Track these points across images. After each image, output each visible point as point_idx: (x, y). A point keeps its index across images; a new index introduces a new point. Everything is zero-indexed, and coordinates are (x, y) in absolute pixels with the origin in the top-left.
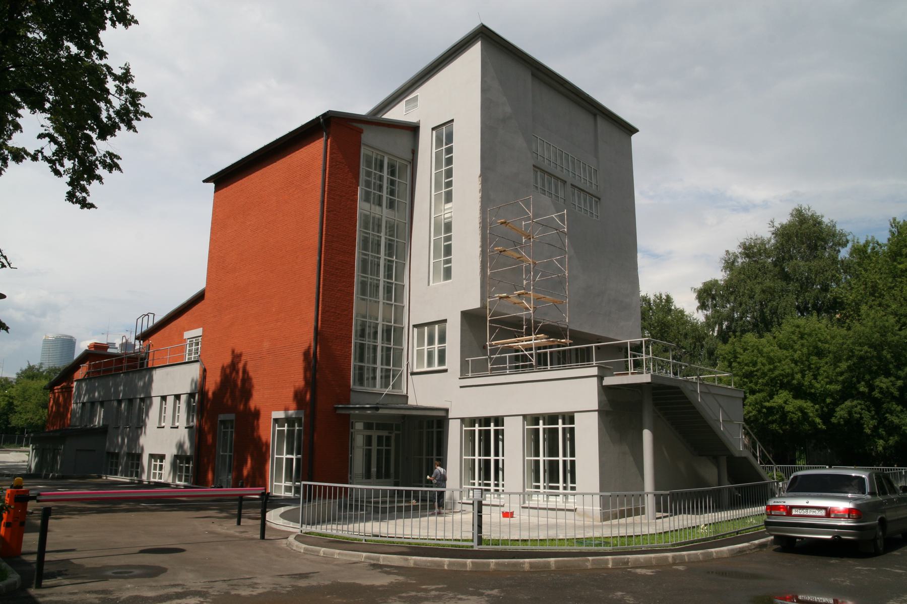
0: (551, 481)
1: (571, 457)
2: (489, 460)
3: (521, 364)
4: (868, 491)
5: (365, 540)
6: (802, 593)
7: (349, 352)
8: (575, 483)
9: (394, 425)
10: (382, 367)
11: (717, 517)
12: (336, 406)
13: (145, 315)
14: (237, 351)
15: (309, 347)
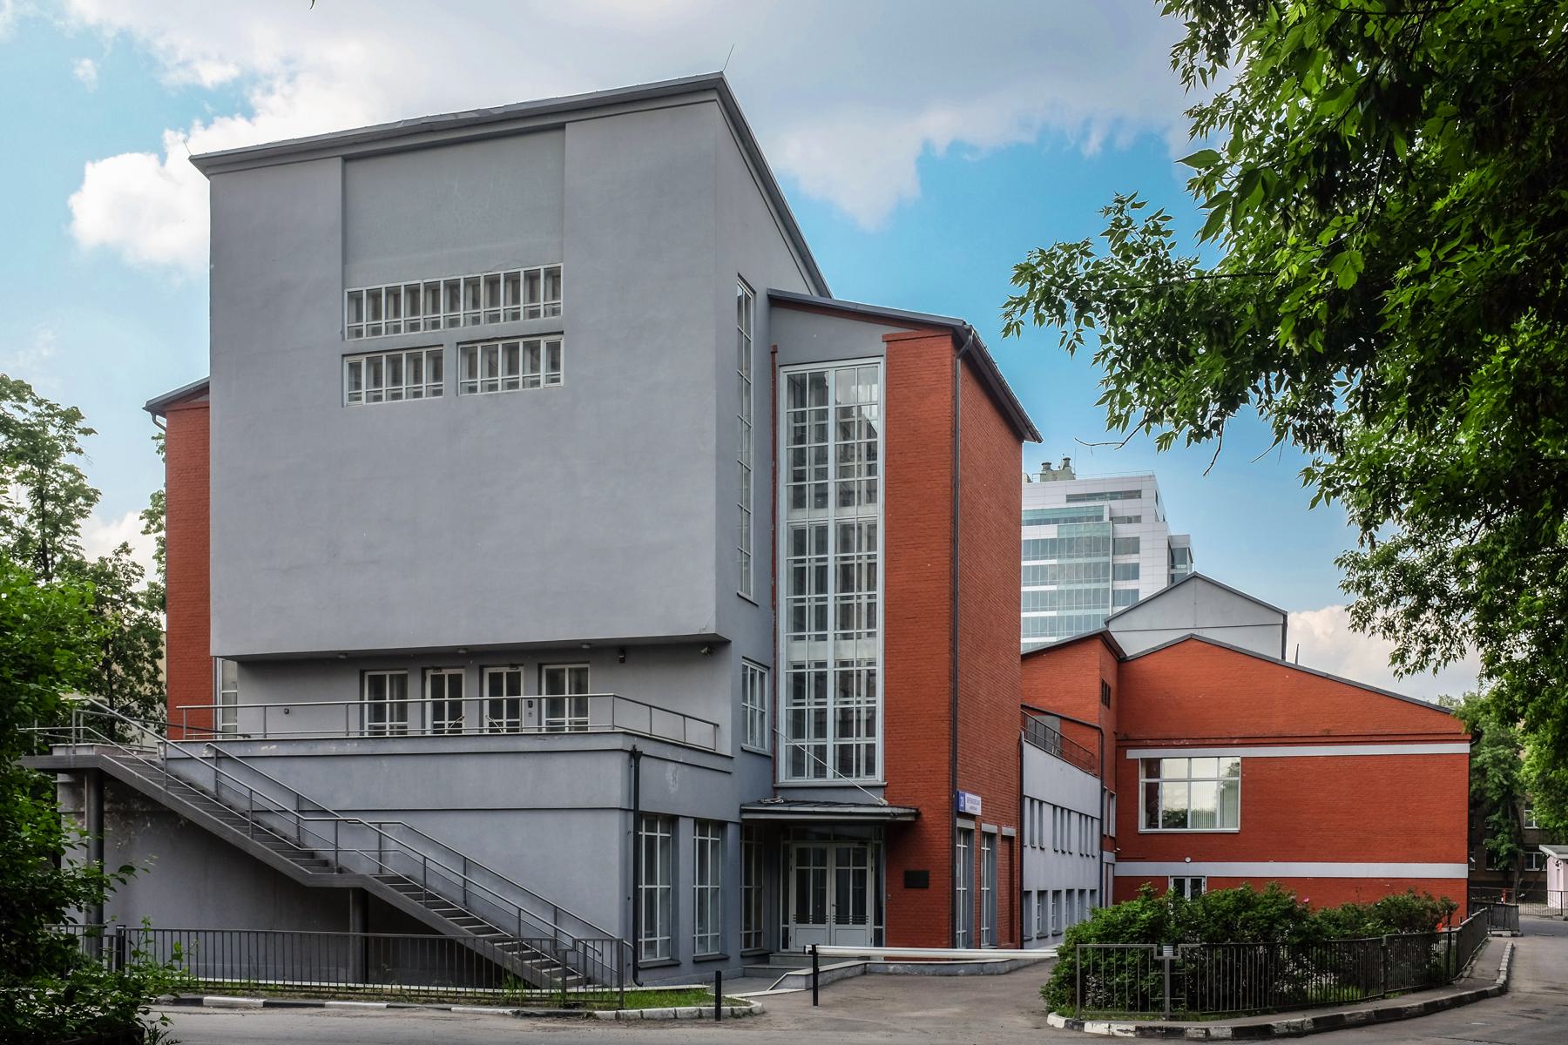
0: (796, 697)
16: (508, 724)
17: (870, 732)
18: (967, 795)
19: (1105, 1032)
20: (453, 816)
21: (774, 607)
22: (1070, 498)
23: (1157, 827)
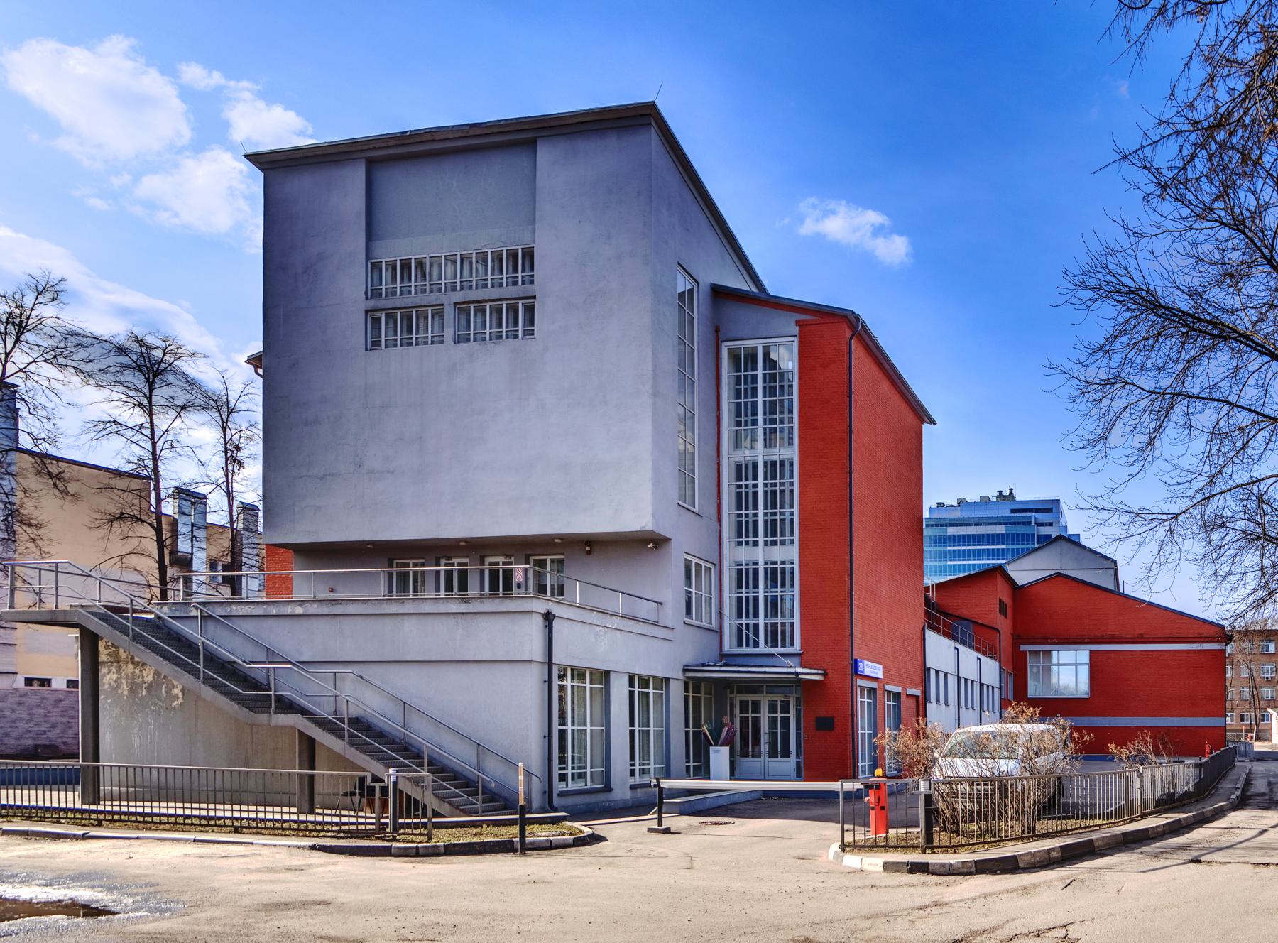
0: (738, 588)
1: (753, 510)
3: (949, 548)
8: (630, 731)
9: (413, 261)
16: (782, 535)
17: (792, 616)
18: (866, 662)
19: (858, 866)
20: (397, 667)
21: (719, 520)
22: (1013, 511)
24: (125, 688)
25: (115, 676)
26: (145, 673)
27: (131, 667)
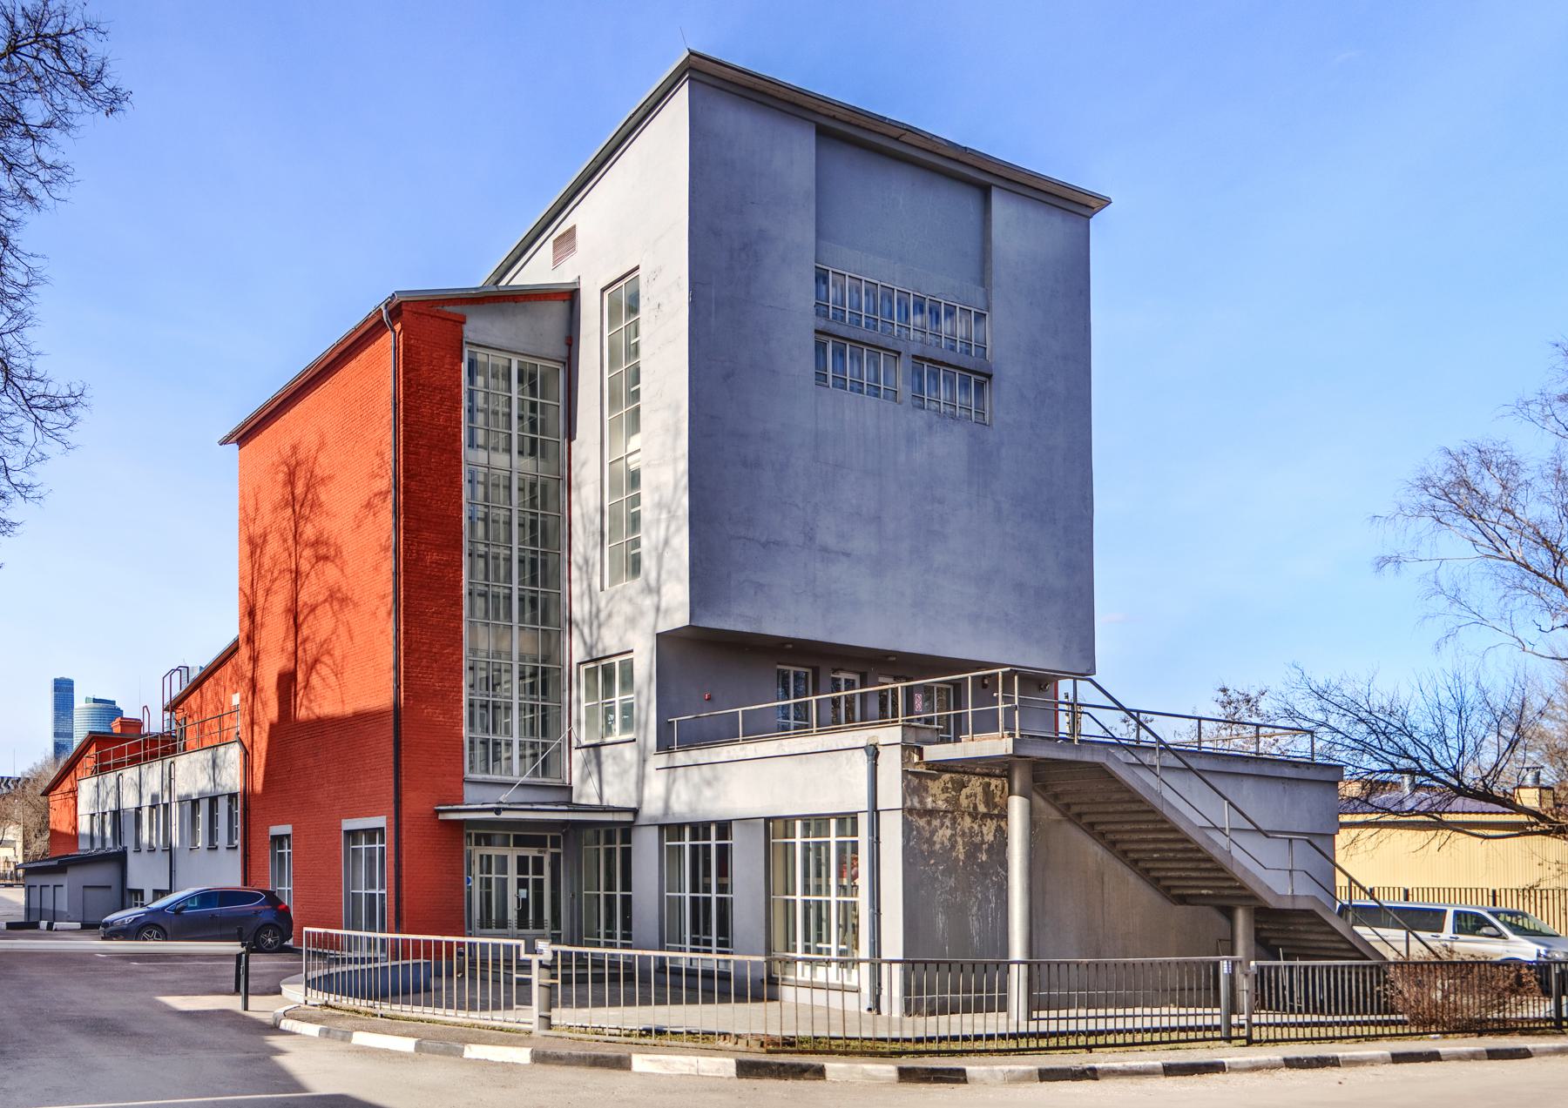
2: (718, 838)
4: (1226, 972)
5: (509, 758)
6: (711, 1085)
7: (460, 717)
10: (482, 876)
11: (1542, 1008)
12: (436, 808)
13: (175, 670)
14: (1438, 468)
15: (315, 1091)
23: (972, 677)
24: (962, 850)
25: (949, 832)
26: (985, 830)
27: (968, 820)
